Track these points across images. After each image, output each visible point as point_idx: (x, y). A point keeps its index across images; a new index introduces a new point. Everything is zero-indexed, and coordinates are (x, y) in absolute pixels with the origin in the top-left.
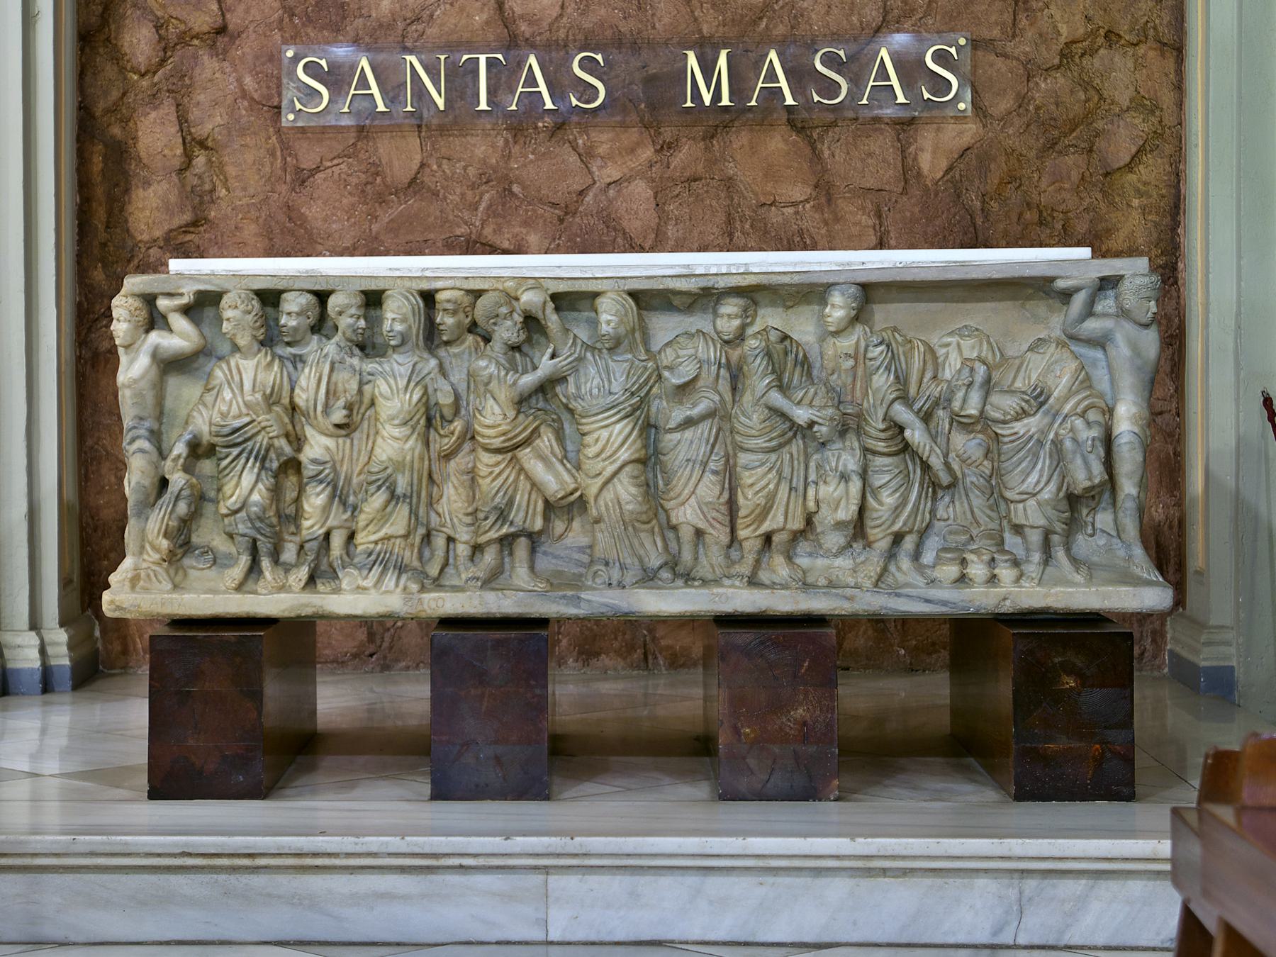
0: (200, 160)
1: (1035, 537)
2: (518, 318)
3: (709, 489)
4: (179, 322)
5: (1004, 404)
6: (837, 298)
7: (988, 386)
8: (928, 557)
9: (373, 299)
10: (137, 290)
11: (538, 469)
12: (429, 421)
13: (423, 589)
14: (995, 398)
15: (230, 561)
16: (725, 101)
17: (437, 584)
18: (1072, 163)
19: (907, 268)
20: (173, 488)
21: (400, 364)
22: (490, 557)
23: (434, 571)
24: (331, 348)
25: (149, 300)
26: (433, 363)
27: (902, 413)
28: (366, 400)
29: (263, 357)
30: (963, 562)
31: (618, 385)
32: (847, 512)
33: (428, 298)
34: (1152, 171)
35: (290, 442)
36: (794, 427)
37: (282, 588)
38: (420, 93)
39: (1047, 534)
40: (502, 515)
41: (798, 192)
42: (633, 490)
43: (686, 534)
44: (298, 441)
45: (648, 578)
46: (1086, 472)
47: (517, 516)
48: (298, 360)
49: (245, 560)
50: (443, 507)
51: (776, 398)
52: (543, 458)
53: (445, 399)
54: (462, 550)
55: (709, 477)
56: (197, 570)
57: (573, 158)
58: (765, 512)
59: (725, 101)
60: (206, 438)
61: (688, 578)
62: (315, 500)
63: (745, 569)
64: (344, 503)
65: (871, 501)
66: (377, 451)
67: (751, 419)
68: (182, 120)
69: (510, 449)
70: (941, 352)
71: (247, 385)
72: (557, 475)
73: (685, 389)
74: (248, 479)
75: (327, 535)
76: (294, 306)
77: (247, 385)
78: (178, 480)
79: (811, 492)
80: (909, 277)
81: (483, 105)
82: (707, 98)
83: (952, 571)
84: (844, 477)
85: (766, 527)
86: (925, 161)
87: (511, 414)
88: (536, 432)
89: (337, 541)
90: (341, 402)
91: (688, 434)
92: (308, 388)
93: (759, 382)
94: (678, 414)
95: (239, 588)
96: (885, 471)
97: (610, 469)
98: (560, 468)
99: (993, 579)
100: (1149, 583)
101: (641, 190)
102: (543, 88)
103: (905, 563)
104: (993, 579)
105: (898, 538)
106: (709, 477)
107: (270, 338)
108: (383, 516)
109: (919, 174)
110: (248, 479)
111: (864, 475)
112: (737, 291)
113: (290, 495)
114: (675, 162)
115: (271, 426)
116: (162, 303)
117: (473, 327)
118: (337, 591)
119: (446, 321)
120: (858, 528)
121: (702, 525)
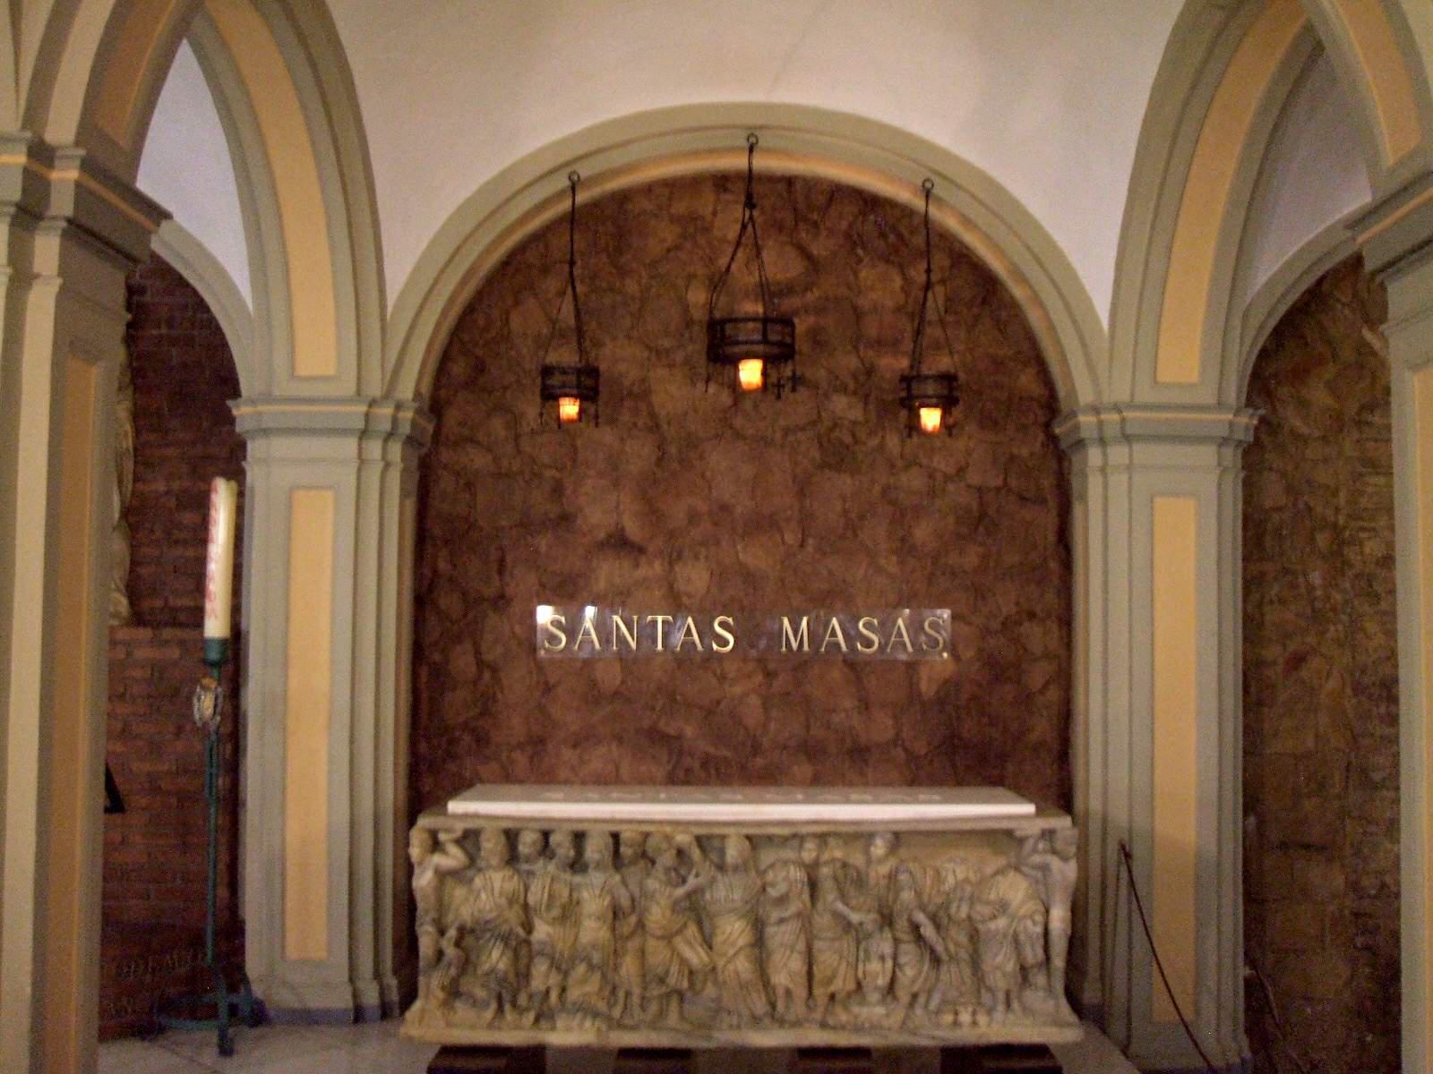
0: (487, 675)
1: (1001, 996)
2: (674, 852)
3: (797, 964)
4: (454, 850)
5: (982, 910)
6: (879, 842)
7: (972, 901)
8: (933, 1005)
9: (579, 838)
10: (427, 826)
11: (688, 953)
12: (615, 914)
13: (610, 1028)
14: (979, 907)
15: (486, 1005)
16: (806, 647)
17: (620, 1026)
18: (1008, 691)
19: (918, 821)
20: (446, 960)
21: (596, 878)
22: (653, 1008)
23: (617, 1012)
24: (551, 867)
25: (433, 834)
26: (617, 878)
27: (921, 917)
28: (574, 903)
29: (508, 872)
30: (956, 1013)
31: (737, 895)
32: (882, 981)
33: (615, 837)
34: (1053, 694)
35: (524, 929)
36: (849, 924)
37: (518, 1027)
38: (622, 640)
39: (1008, 994)
40: (662, 981)
41: (848, 703)
42: (747, 964)
43: (780, 992)
44: (529, 928)
45: (756, 1021)
46: (1033, 954)
47: (672, 981)
48: (530, 873)
49: (494, 1006)
50: (623, 972)
51: (840, 906)
52: (690, 944)
53: (625, 902)
54: (636, 1000)
55: (795, 955)
56: (462, 1010)
57: (714, 681)
58: (830, 981)
59: (806, 647)
60: (469, 925)
61: (781, 1022)
62: (540, 968)
63: (818, 1015)
64: (558, 969)
65: (899, 973)
66: (581, 934)
67: (823, 921)
68: (478, 653)
69: (668, 938)
70: (944, 873)
71: (497, 894)
72: (698, 954)
73: (782, 900)
74: (495, 954)
75: (548, 992)
76: (527, 842)
77: (497, 894)
78: (450, 951)
79: (861, 967)
80: (922, 827)
81: (660, 647)
82: (795, 645)
83: (949, 1018)
84: (882, 958)
85: (832, 988)
86: (924, 686)
87: (668, 913)
88: (685, 925)
89: (554, 996)
90: (558, 903)
91: (783, 928)
92: (536, 895)
93: (829, 895)
94: (775, 915)
95: (490, 1026)
96: (909, 953)
97: (731, 952)
98: (700, 949)
99: (975, 1023)
100: (1069, 1025)
101: (754, 700)
102: (696, 636)
103: (919, 1011)
104: (975, 1023)
105: (915, 996)
106: (795, 955)
107: (512, 858)
108: (584, 981)
109: (920, 694)
110: (495, 954)
111: (895, 958)
112: (815, 835)
113: (524, 961)
114: (775, 684)
115: (513, 917)
116: (442, 837)
117: (644, 855)
118: (553, 1028)
119: (626, 851)
120: (891, 988)
121: (791, 986)
